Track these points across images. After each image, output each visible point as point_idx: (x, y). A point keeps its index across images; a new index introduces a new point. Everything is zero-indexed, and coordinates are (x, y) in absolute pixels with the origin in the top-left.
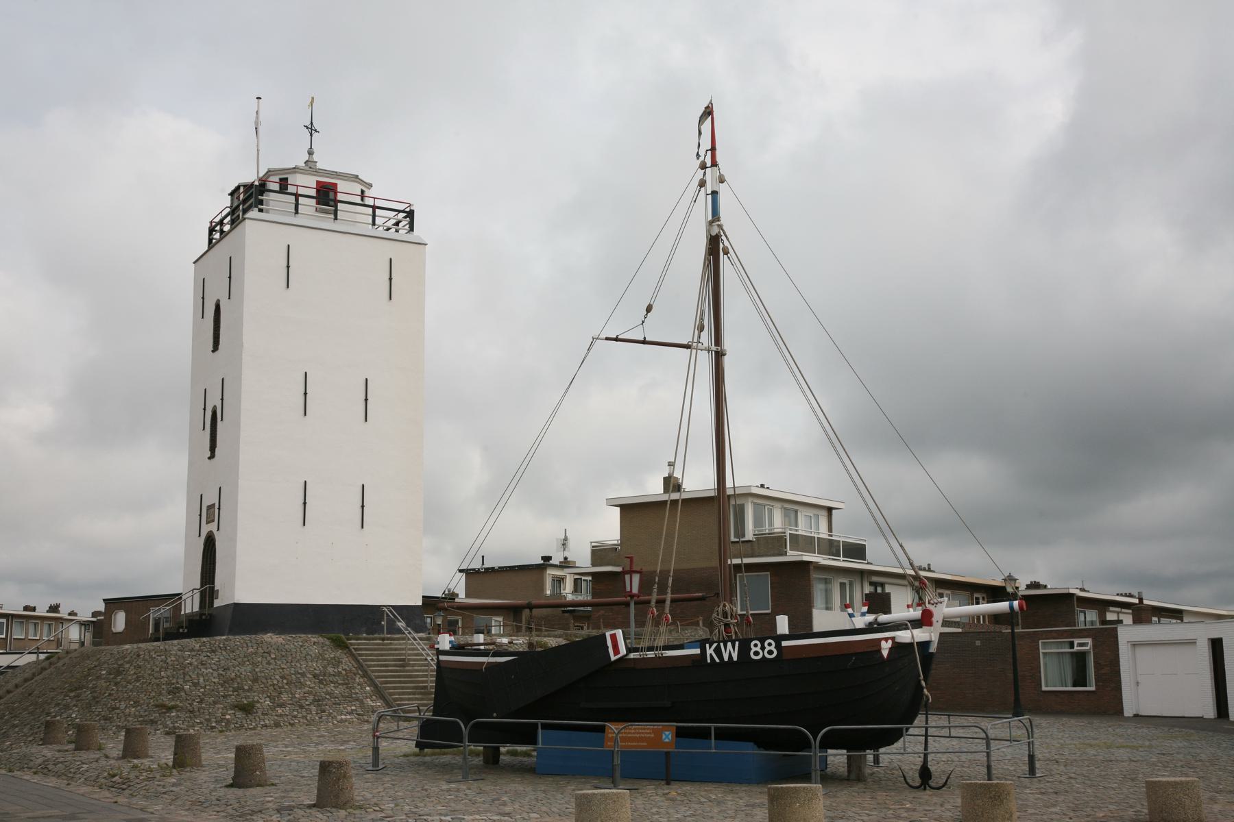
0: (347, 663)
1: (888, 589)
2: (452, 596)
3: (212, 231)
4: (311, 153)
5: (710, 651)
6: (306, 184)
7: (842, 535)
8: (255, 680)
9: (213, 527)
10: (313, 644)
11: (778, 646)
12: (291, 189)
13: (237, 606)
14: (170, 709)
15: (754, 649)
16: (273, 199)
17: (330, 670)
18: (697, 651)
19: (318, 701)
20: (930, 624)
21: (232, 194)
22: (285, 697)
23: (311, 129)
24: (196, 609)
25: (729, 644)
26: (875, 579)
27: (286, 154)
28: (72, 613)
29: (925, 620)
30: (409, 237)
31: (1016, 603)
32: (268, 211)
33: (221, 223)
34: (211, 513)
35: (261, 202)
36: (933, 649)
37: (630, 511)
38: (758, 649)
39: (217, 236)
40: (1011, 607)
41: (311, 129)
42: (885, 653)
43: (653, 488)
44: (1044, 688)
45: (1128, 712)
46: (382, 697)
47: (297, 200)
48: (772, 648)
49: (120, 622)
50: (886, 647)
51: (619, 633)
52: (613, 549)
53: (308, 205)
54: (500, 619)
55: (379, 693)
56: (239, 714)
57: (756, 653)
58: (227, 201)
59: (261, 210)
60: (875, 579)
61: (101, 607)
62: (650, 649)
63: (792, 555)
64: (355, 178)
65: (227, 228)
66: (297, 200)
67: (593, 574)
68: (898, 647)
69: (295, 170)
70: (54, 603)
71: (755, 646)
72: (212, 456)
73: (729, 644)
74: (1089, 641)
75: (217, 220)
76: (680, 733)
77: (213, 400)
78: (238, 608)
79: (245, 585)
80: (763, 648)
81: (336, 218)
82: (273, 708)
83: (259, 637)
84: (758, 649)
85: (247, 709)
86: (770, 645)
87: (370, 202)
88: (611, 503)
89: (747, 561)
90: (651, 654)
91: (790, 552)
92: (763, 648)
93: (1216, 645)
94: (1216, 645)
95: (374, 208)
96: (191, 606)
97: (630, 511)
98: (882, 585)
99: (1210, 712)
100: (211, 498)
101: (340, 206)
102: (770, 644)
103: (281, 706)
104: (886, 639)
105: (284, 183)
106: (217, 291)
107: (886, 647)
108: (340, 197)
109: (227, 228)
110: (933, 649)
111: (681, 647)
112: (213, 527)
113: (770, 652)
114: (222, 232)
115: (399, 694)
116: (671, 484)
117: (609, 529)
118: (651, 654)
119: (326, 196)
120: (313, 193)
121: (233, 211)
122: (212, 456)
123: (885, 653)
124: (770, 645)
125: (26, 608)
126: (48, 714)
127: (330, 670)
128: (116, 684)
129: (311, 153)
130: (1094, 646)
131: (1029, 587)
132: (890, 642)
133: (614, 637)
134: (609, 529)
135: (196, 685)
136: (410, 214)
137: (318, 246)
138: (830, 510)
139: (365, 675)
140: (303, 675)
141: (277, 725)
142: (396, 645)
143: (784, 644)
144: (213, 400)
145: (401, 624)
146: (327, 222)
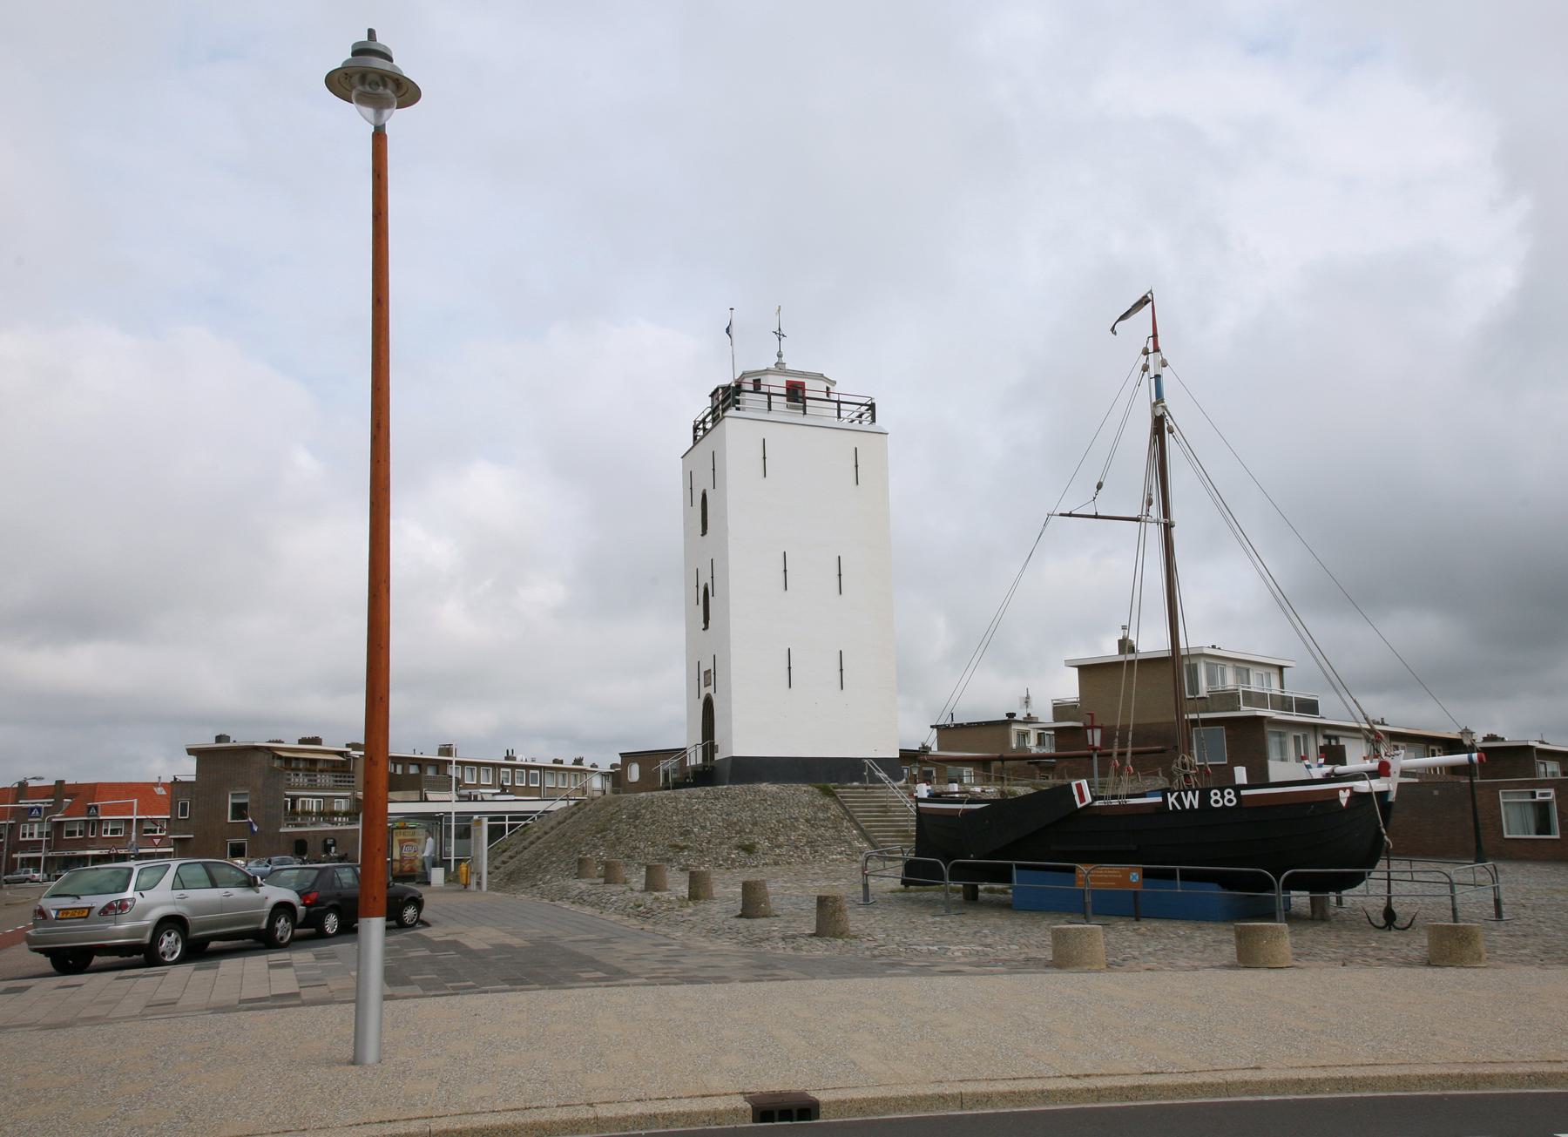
0: (835, 809)
1: (1342, 742)
3: (696, 429)
4: (780, 356)
5: (1171, 799)
6: (777, 383)
8: (755, 824)
9: (710, 690)
10: (804, 792)
11: (1237, 795)
12: (763, 389)
14: (682, 849)
18: (1160, 799)
19: (811, 843)
20: (1388, 775)
21: (712, 395)
22: (781, 839)
23: (780, 334)
24: (700, 761)
26: (1328, 732)
30: (872, 428)
31: (1475, 756)
33: (704, 421)
34: (708, 705)
36: (1392, 798)
39: (701, 433)
40: (1470, 759)
41: (780, 334)
42: (1344, 802)
43: (1108, 650)
46: (868, 840)
48: (1232, 796)
49: (634, 773)
50: (1344, 797)
51: (1084, 782)
52: (1073, 707)
53: (780, 403)
55: (865, 835)
56: (743, 854)
57: (1217, 802)
58: (708, 402)
60: (1328, 732)
61: (618, 761)
62: (1114, 797)
63: (1245, 711)
64: (821, 377)
65: (709, 426)
68: (1356, 797)
69: (767, 372)
71: (1215, 795)
72: (704, 532)
74: (1552, 791)
78: (736, 761)
79: (743, 738)
80: (1223, 797)
82: (771, 849)
83: (756, 786)
85: (749, 849)
86: (1230, 794)
87: (833, 397)
89: (1202, 716)
92: (1223, 797)
95: (839, 402)
96: (695, 759)
98: (1336, 738)
103: (779, 847)
104: (1344, 789)
106: (704, 481)
107: (1344, 797)
108: (808, 394)
109: (709, 426)
111: (1143, 795)
112: (710, 690)
113: (1230, 801)
116: (1125, 646)
118: (1115, 802)
119: (795, 393)
120: (784, 391)
121: (714, 410)
123: (1344, 802)
124: (1230, 794)
125: (555, 761)
127: (821, 815)
129: (780, 356)
130: (1557, 796)
133: (1079, 786)
134: (1069, 688)
135: (703, 828)
136: (872, 407)
139: (852, 819)
140: (796, 819)
141: (776, 863)
142: (878, 793)
143: (1243, 793)
144: (705, 578)
145: (882, 775)
146: (797, 417)
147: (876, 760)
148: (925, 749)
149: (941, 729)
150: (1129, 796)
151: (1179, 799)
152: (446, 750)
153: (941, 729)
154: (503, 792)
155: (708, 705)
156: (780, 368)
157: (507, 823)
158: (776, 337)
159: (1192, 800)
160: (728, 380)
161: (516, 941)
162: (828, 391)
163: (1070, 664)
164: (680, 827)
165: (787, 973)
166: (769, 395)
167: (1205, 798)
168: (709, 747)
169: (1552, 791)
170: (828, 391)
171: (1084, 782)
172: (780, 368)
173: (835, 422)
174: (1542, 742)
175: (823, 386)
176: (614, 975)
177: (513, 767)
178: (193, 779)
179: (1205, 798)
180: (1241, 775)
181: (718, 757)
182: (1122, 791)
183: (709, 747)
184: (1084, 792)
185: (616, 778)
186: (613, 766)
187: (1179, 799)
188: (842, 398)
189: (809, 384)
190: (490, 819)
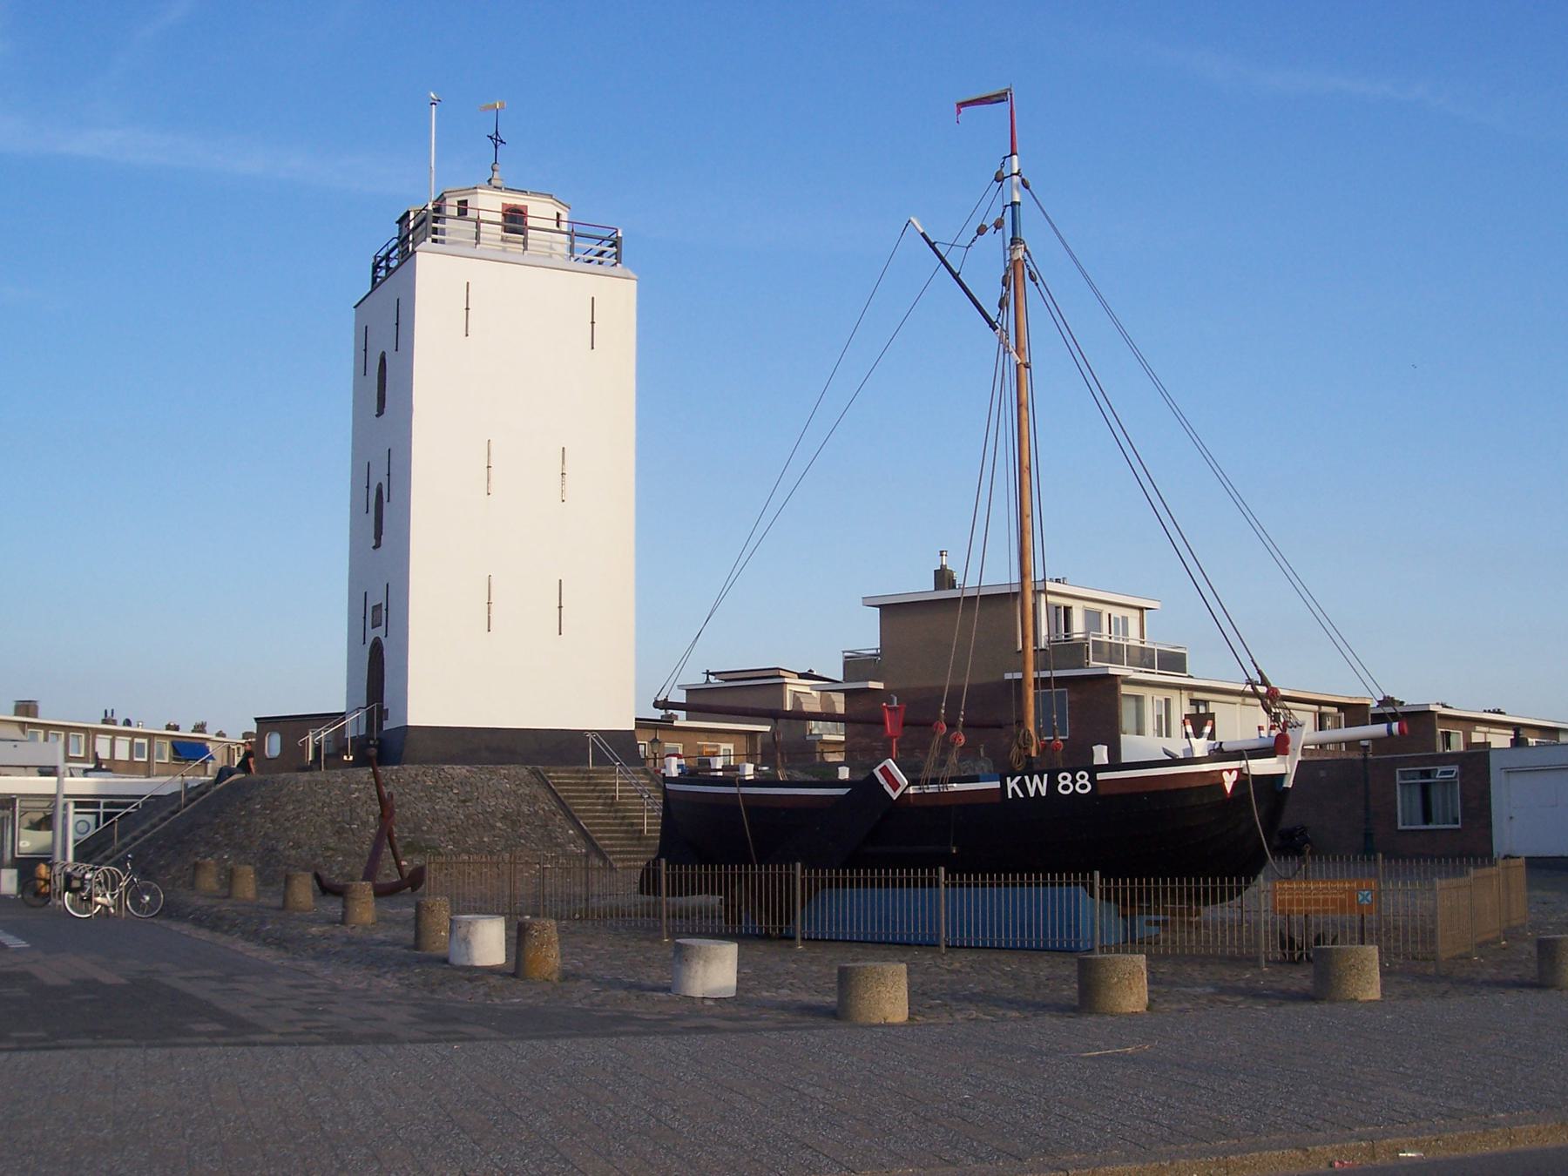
1: (1212, 708)
3: (376, 267)
5: (1012, 784)
7: (1158, 642)
11: (1092, 779)
12: (471, 214)
15: (1062, 783)
16: (453, 227)
17: (525, 809)
18: (997, 785)
20: (1285, 753)
21: (399, 222)
25: (1036, 778)
26: (1198, 695)
28: (220, 734)
29: (1278, 747)
31: (1395, 726)
32: (443, 242)
33: (387, 257)
34: (377, 651)
36: (1289, 783)
37: (891, 611)
38: (1068, 782)
39: (382, 273)
40: (1389, 730)
42: (1229, 787)
43: (921, 585)
44: (1400, 827)
47: (478, 227)
48: (1085, 781)
49: (273, 745)
50: (1229, 781)
51: (890, 763)
53: (493, 232)
54: (730, 746)
57: (1066, 787)
59: (435, 241)
60: (1198, 695)
61: (253, 728)
62: (934, 781)
63: (1095, 666)
65: (393, 264)
66: (478, 227)
67: (847, 692)
68: (1243, 778)
70: (199, 722)
71: (1064, 778)
72: (380, 412)
73: (1036, 778)
74: (1456, 768)
75: (382, 254)
80: (1074, 782)
84: (1068, 782)
86: (1083, 778)
88: (868, 602)
89: (1057, 673)
90: (932, 788)
91: (1093, 663)
92: (1074, 782)
97: (891, 611)
98: (1206, 703)
100: (377, 598)
102: (1082, 777)
104: (1230, 771)
107: (1229, 781)
109: (393, 264)
110: (1288, 783)
111: (976, 779)
113: (1083, 787)
114: (388, 268)
115: (610, 839)
116: (943, 578)
117: (867, 637)
118: (932, 788)
120: (499, 218)
121: (403, 241)
122: (380, 412)
123: (1229, 787)
124: (1083, 778)
125: (169, 727)
126: (197, 854)
128: (273, 821)
130: (1462, 775)
131: (1381, 704)
132: (1235, 773)
133: (885, 771)
134: (867, 637)
138: (1141, 609)
143: (1100, 776)
144: (379, 476)
150: (952, 780)
151: (1022, 784)
154: (98, 768)
155: (377, 651)
157: (102, 810)
159: (1038, 785)
161: (107, 978)
163: (868, 602)
164: (333, 822)
165: (179, 1040)
166: (478, 222)
167: (1053, 784)
169: (1456, 768)
174: (1444, 706)
176: (238, 1030)
179: (1053, 784)
180: (1101, 754)
181: (387, 726)
182: (946, 772)
184: (896, 779)
185: (253, 750)
186: (246, 735)
187: (1022, 784)
190: (77, 805)
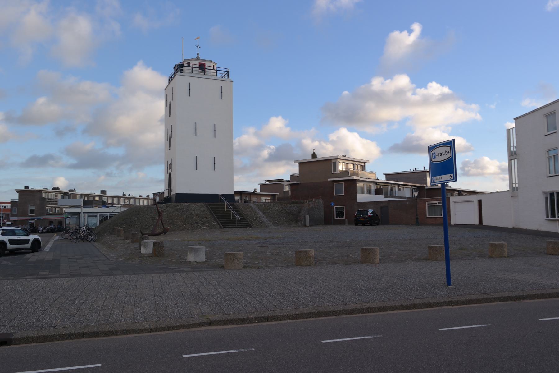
2: (255, 191)
4: (198, 54)
6: (196, 63)
12: (191, 65)
13: (177, 194)
23: (198, 47)
27: (190, 54)
30: (228, 80)
34: (170, 166)
35: (182, 70)
41: (198, 47)
45: (452, 223)
51: (427, 203)
52: (297, 176)
69: (193, 59)
76: (508, 131)
77: (170, 132)
78: (177, 195)
79: (179, 189)
81: (204, 73)
87: (215, 69)
93: (480, 202)
94: (480, 202)
96: (166, 195)
99: (477, 223)
101: (206, 70)
105: (189, 63)
106: (170, 99)
108: (206, 67)
119: (202, 67)
120: (198, 66)
129: (198, 54)
134: (295, 170)
136: (228, 72)
137: (199, 83)
144: (170, 132)
147: (223, 194)
148: (255, 191)
149: (262, 186)
152: (104, 192)
153: (262, 186)
156: (198, 58)
158: (196, 48)
160: (180, 62)
162: (214, 67)
168: (170, 190)
170: (214, 67)
171: (427, 203)
172: (198, 58)
173: (214, 77)
175: (212, 65)
177: (126, 198)
178: (17, 201)
181: (172, 193)
183: (170, 190)
188: (194, 66)
189: (207, 64)
